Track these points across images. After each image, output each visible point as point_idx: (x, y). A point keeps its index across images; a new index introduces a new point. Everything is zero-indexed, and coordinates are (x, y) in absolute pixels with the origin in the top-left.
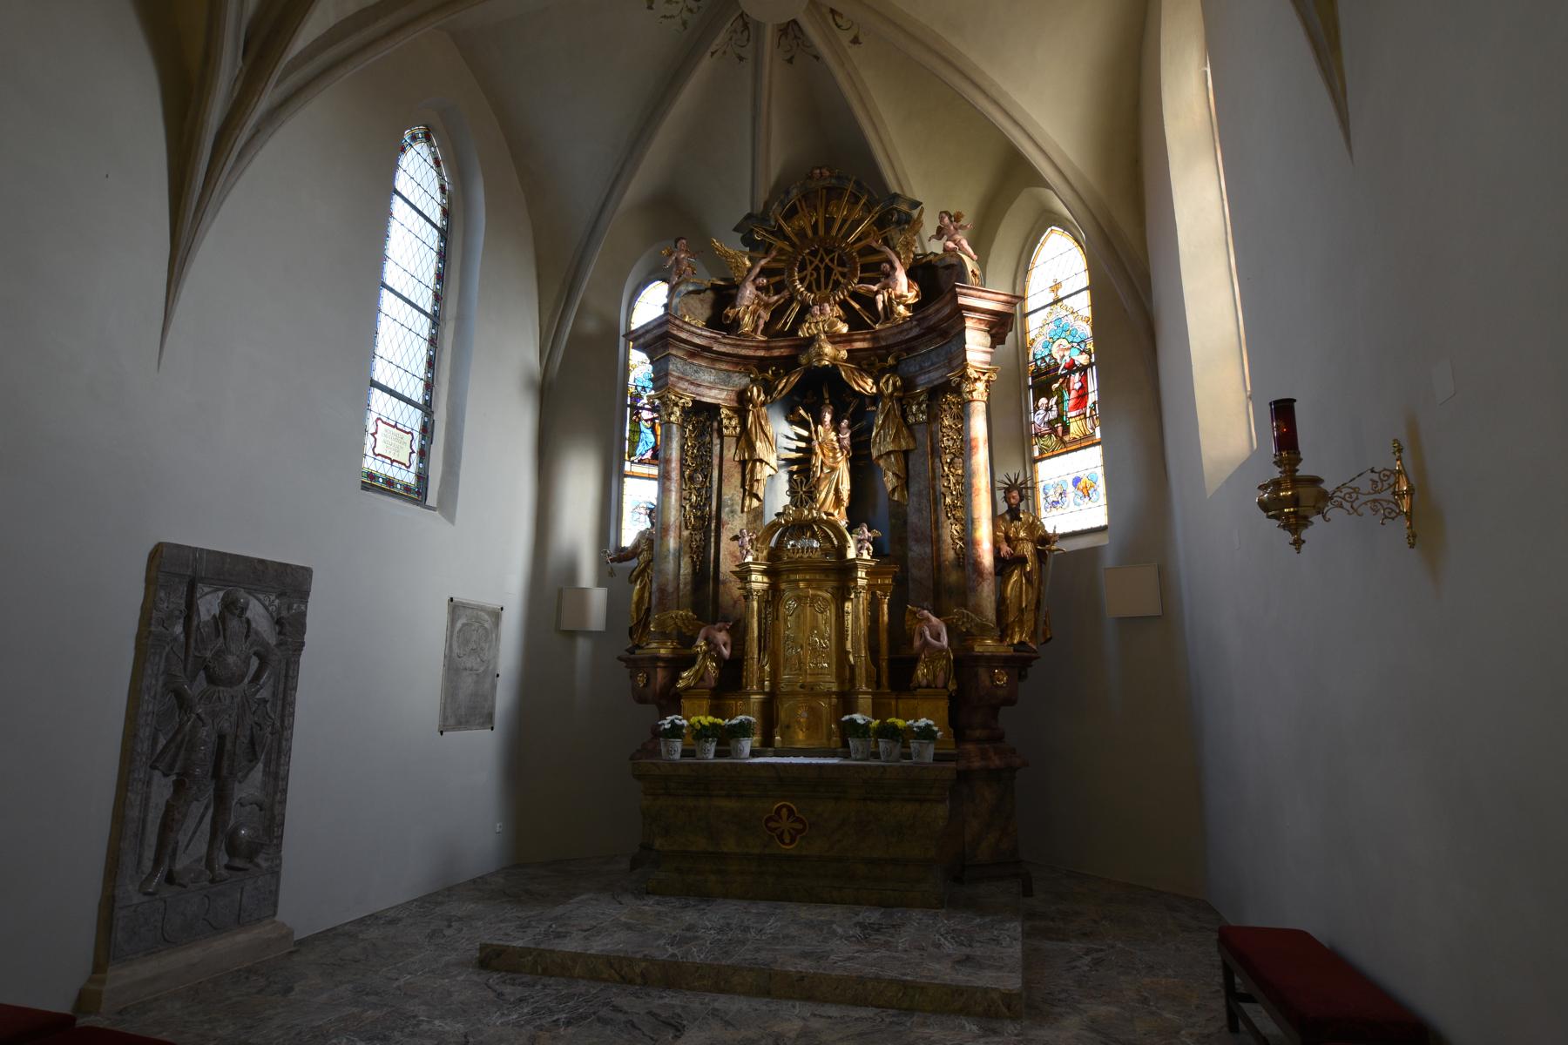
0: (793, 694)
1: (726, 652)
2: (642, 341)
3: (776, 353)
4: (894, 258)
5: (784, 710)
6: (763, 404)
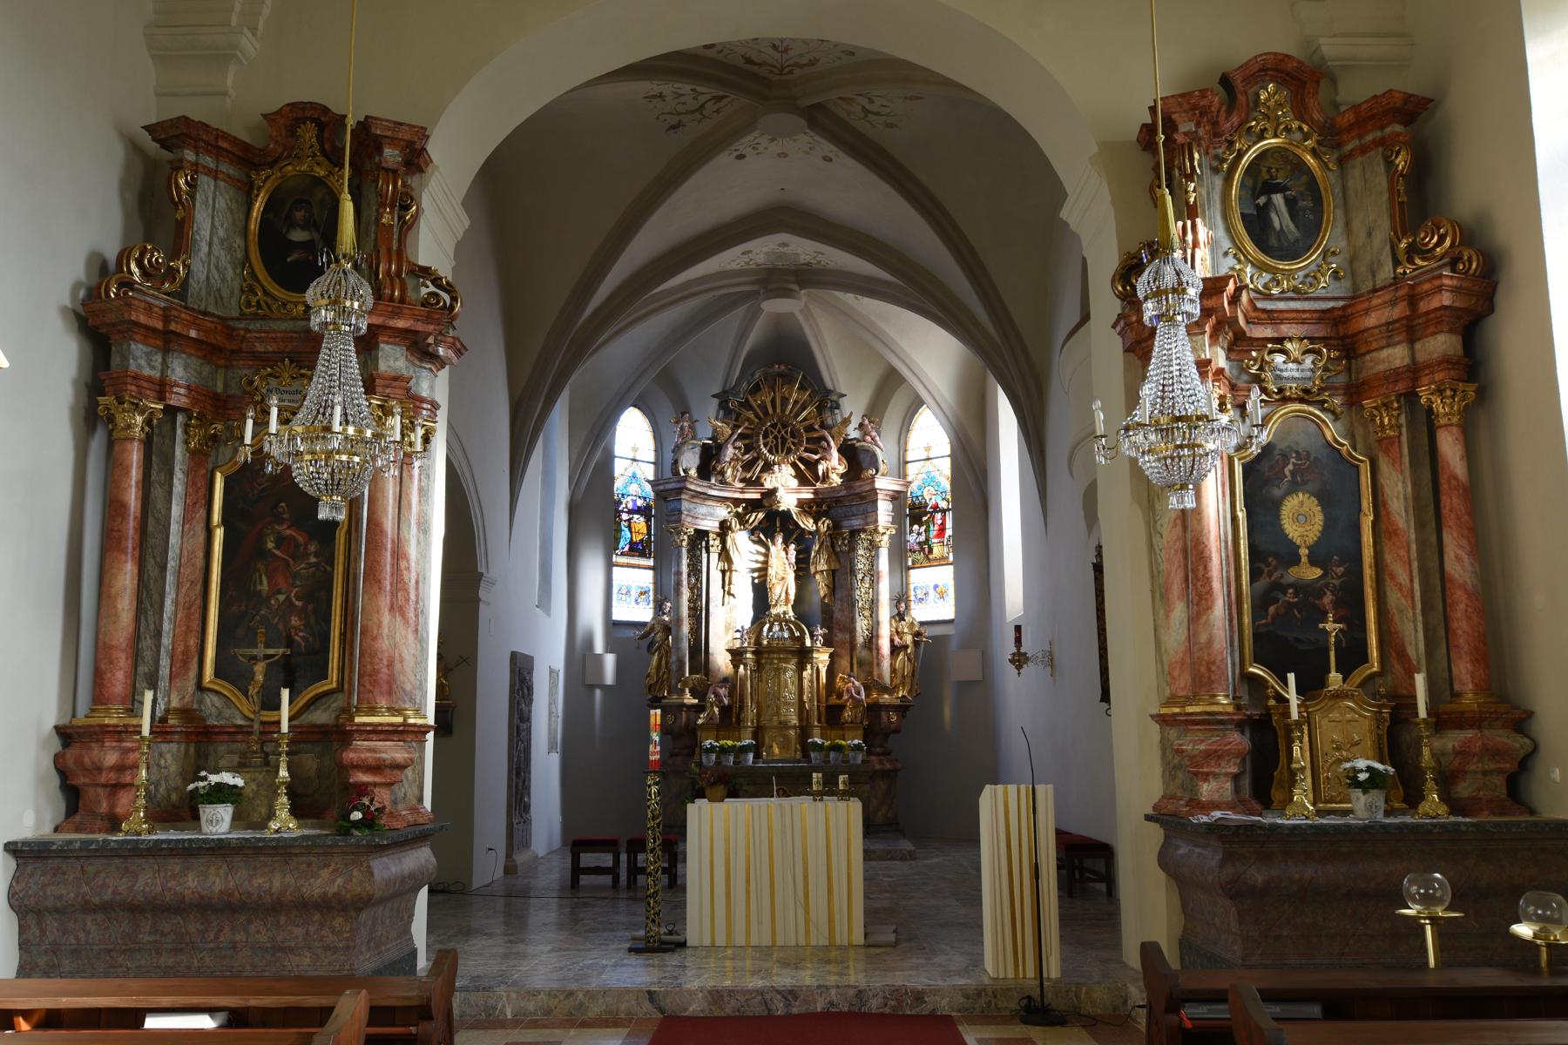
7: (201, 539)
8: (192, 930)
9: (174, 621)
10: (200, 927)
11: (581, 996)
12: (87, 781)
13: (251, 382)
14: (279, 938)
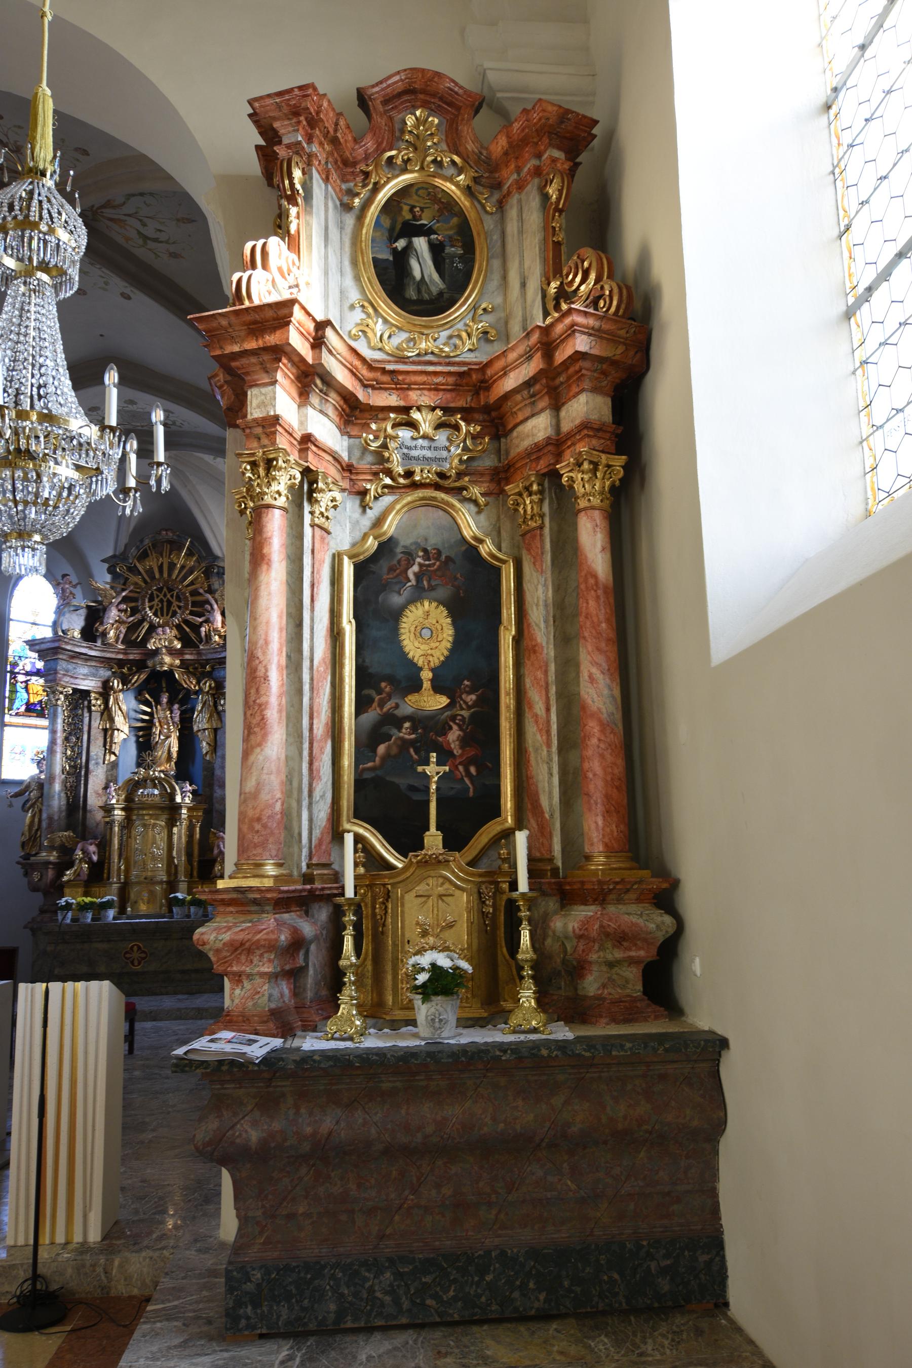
0: (138, 883)
1: (95, 858)
2: (37, 647)
3: (131, 657)
4: (213, 602)
5: (133, 893)
6: (121, 691)
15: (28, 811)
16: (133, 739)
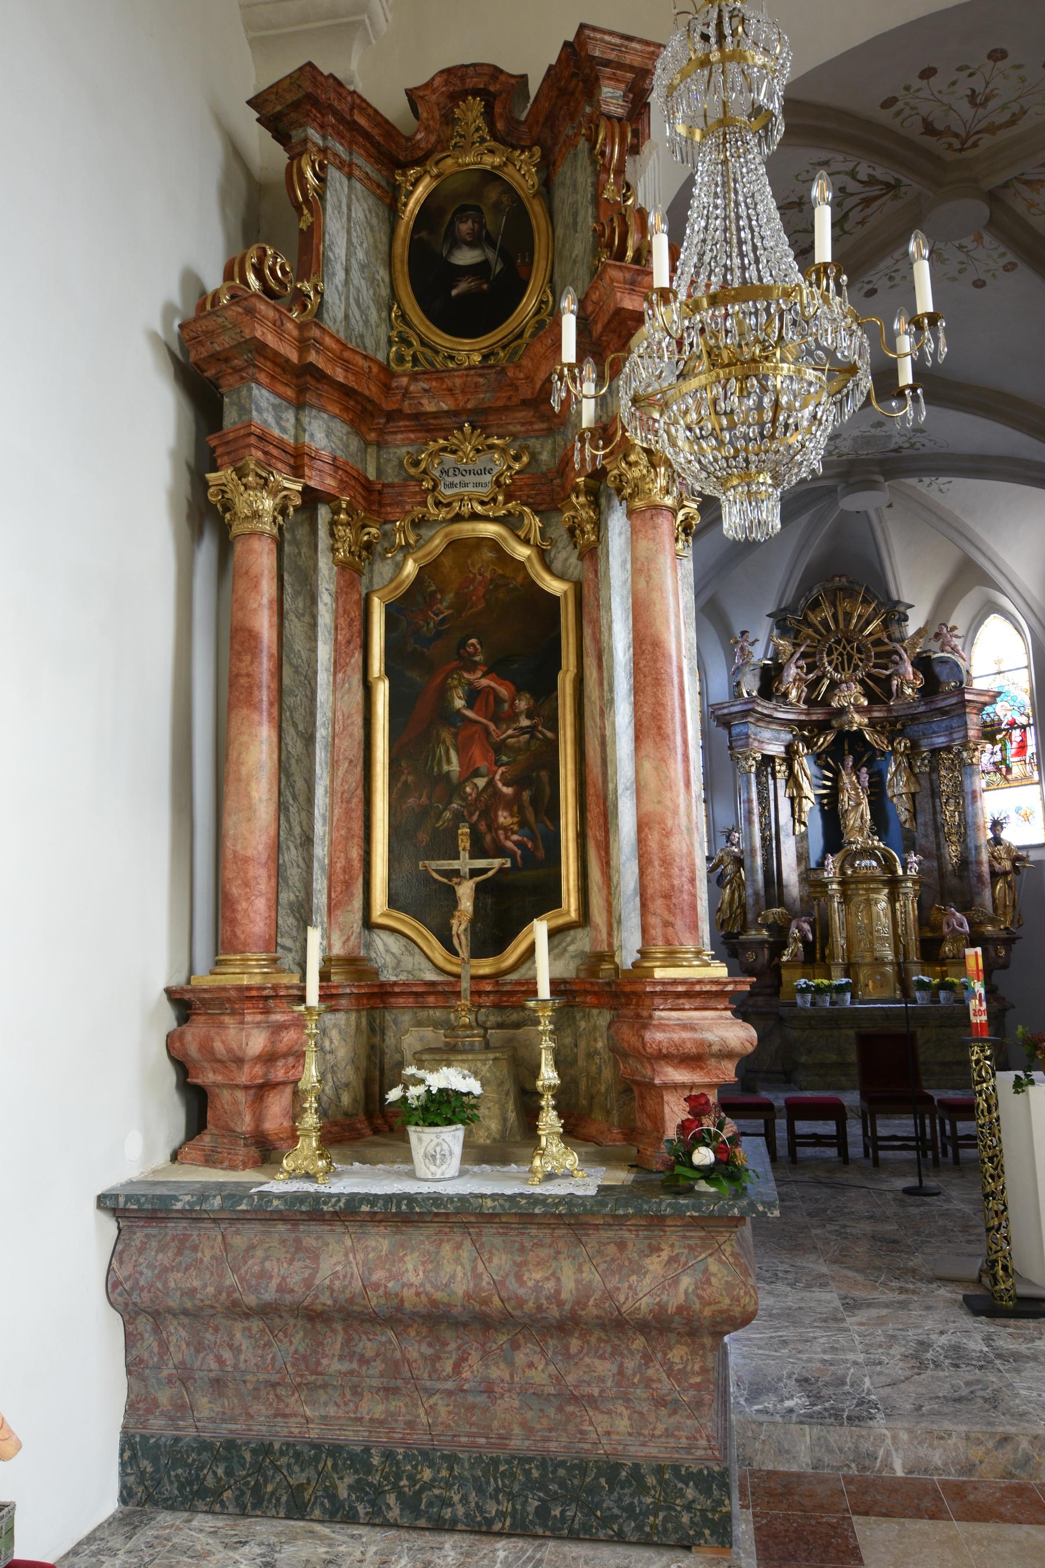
3: (814, 717)
4: (903, 652)
7: (358, 695)
8: (413, 1353)
9: (329, 820)
10: (428, 1351)
11: (1024, 1444)
12: (219, 1078)
13: (416, 463)
14: (570, 1379)
15: (725, 888)
16: (818, 807)
